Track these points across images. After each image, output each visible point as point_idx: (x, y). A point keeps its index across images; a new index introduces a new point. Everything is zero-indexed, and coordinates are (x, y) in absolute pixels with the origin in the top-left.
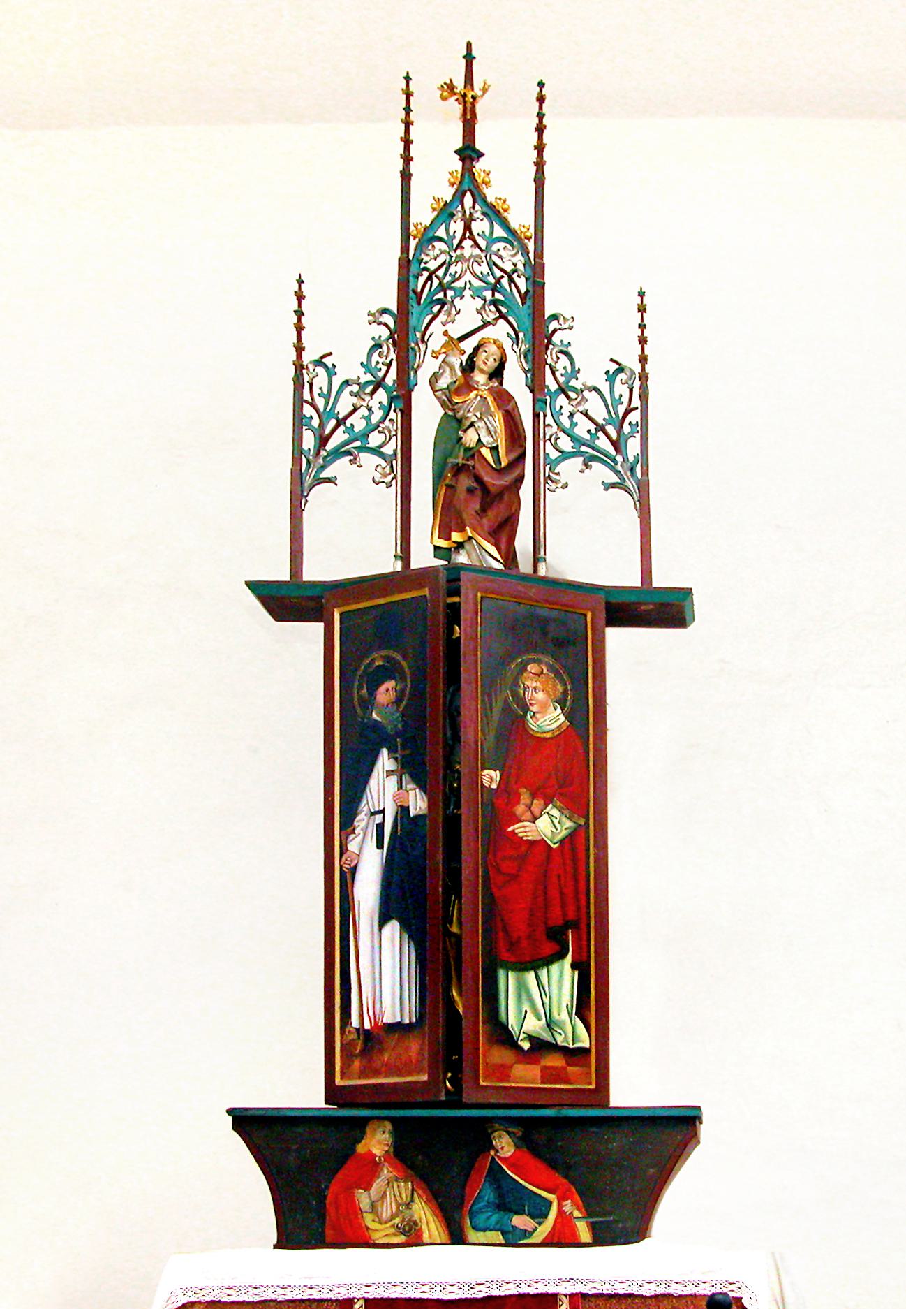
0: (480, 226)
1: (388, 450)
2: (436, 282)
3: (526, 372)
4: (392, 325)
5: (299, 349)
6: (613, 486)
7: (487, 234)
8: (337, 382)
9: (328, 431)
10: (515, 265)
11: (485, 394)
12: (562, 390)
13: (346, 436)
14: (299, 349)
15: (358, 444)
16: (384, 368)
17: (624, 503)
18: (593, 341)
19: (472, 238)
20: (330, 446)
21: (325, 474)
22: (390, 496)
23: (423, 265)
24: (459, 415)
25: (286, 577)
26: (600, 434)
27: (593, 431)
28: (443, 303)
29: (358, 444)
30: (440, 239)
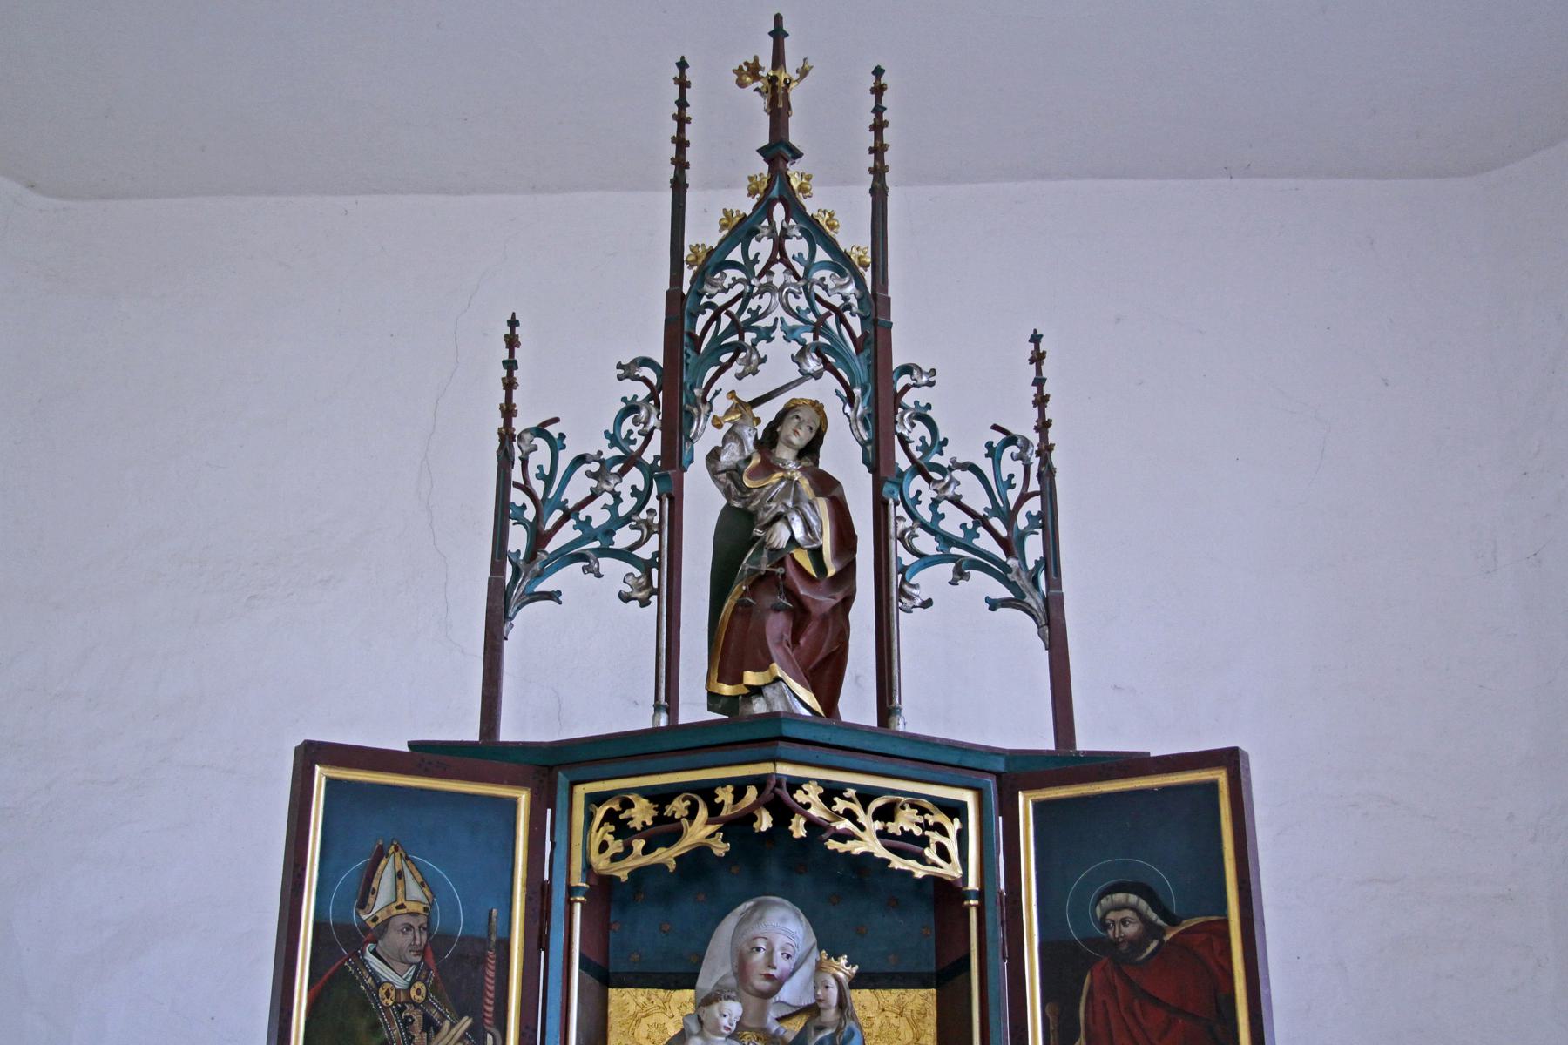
0: (796, 246)
1: (645, 553)
2: (726, 321)
3: (863, 444)
4: (654, 381)
5: (508, 412)
6: (1005, 603)
7: (806, 256)
8: (565, 459)
9: (549, 526)
10: (845, 298)
11: (797, 476)
12: (919, 469)
13: (578, 533)
14: (508, 412)
15: (597, 544)
16: (641, 440)
17: (1022, 627)
18: (965, 400)
19: (784, 259)
20: (551, 547)
21: (545, 586)
22: (647, 618)
23: (705, 300)
24: (751, 507)
25: (472, 734)
26: (981, 530)
27: (970, 526)
28: (738, 348)
29: (597, 544)
30: (734, 265)
